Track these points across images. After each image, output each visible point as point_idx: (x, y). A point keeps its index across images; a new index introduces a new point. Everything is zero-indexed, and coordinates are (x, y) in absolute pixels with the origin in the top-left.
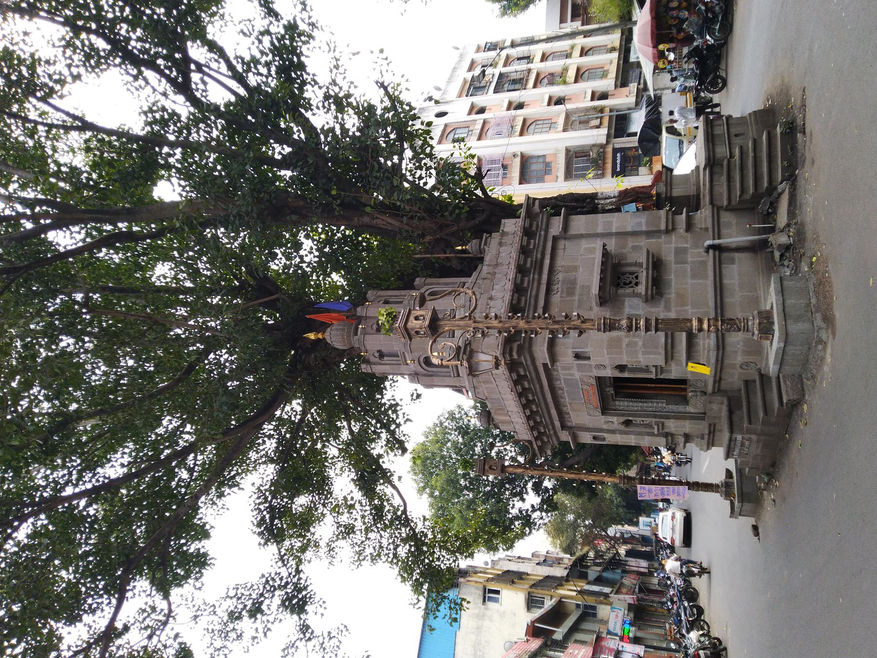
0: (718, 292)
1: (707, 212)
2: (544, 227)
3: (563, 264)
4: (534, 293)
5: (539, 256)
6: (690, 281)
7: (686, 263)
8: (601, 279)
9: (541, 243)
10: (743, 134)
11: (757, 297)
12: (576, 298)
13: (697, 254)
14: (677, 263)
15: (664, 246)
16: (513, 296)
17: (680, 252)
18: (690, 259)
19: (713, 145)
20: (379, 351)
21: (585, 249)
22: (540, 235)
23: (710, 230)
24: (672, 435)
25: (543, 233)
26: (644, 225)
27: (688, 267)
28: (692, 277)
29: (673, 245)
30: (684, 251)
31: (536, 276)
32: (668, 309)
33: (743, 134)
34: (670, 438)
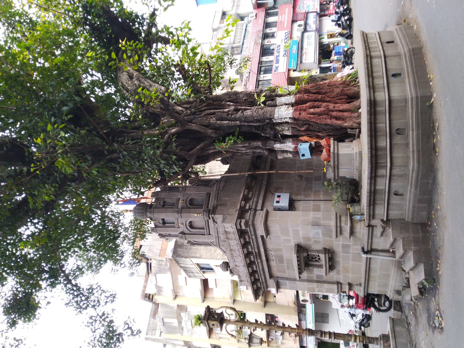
0: (367, 281)
1: (365, 231)
2: (253, 233)
3: (272, 247)
4: (261, 268)
5: (257, 251)
6: (351, 262)
7: (349, 253)
8: (298, 265)
9: (255, 243)
10: (402, 195)
11: (389, 275)
12: (285, 264)
13: (356, 249)
14: (344, 253)
15: (335, 243)
16: (248, 270)
17: (345, 247)
18: (351, 251)
19: (374, 204)
20: (163, 220)
21: (284, 239)
22: (252, 239)
23: (363, 285)
24: (341, 284)
25: (254, 237)
26: (321, 234)
27: (351, 255)
28: (353, 261)
29: (341, 243)
30: (348, 246)
31: (259, 261)
32: (338, 273)
33: (402, 195)
34: (340, 285)
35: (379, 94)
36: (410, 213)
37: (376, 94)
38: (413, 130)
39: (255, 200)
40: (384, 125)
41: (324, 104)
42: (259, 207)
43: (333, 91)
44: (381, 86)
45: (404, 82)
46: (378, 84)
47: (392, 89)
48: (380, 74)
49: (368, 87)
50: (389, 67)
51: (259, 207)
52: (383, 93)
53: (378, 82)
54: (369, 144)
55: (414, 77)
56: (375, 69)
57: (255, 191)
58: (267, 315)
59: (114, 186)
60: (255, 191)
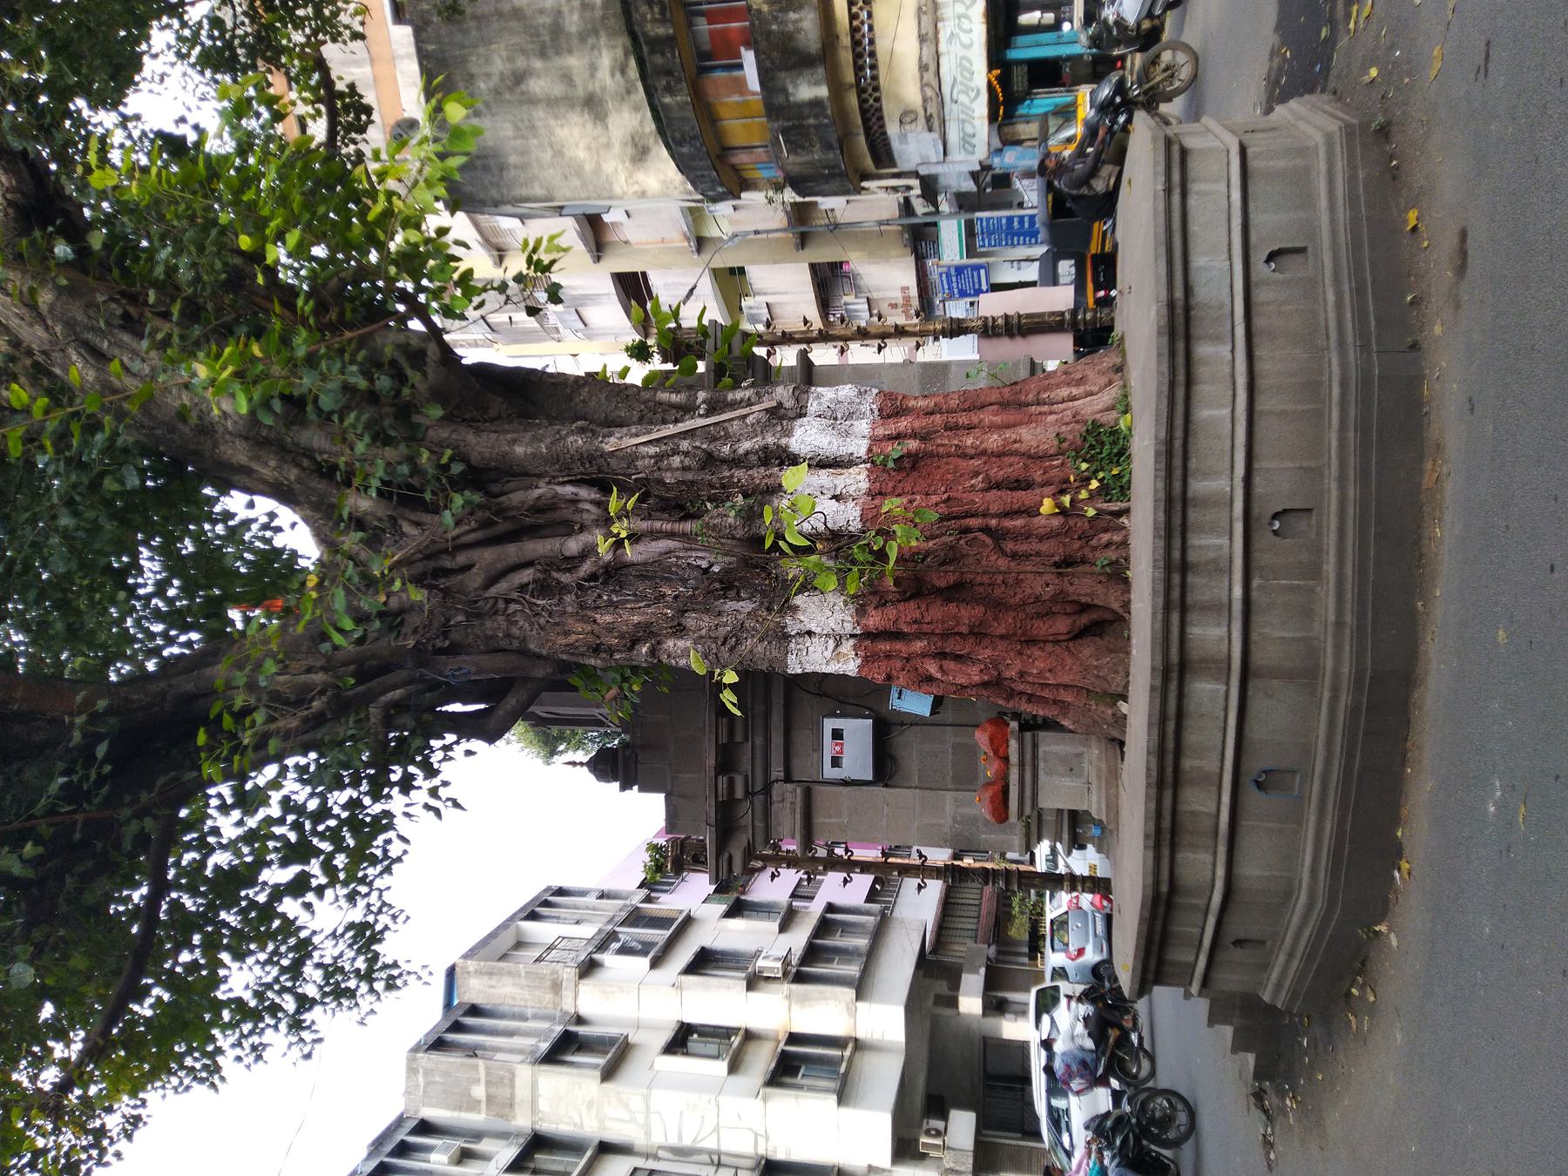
35: (1191, 856)
36: (1342, 214)
37: (1181, 856)
38: (1291, 955)
39: (759, 741)
40: (1196, 931)
41: (985, 653)
42: (777, 772)
43: (1018, 582)
44: (1207, 823)
45: (1298, 819)
46: (1193, 813)
47: (1246, 843)
48: (1211, 765)
49: (1151, 843)
50: (1255, 731)
51: (777, 772)
52: (1207, 857)
53: (1196, 801)
54: (1159, 650)
55: (1341, 823)
56: (1192, 737)
57: (753, 704)
58: (813, 267)
59: (261, 742)
60: (753, 704)
